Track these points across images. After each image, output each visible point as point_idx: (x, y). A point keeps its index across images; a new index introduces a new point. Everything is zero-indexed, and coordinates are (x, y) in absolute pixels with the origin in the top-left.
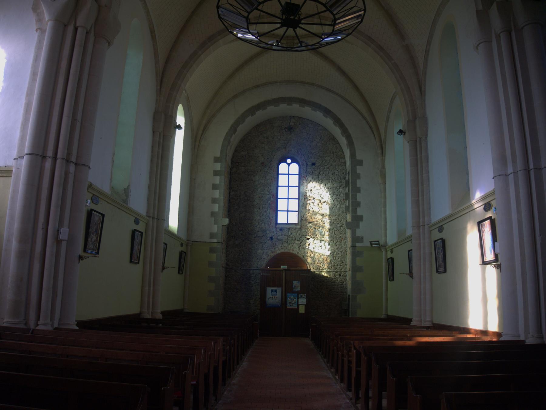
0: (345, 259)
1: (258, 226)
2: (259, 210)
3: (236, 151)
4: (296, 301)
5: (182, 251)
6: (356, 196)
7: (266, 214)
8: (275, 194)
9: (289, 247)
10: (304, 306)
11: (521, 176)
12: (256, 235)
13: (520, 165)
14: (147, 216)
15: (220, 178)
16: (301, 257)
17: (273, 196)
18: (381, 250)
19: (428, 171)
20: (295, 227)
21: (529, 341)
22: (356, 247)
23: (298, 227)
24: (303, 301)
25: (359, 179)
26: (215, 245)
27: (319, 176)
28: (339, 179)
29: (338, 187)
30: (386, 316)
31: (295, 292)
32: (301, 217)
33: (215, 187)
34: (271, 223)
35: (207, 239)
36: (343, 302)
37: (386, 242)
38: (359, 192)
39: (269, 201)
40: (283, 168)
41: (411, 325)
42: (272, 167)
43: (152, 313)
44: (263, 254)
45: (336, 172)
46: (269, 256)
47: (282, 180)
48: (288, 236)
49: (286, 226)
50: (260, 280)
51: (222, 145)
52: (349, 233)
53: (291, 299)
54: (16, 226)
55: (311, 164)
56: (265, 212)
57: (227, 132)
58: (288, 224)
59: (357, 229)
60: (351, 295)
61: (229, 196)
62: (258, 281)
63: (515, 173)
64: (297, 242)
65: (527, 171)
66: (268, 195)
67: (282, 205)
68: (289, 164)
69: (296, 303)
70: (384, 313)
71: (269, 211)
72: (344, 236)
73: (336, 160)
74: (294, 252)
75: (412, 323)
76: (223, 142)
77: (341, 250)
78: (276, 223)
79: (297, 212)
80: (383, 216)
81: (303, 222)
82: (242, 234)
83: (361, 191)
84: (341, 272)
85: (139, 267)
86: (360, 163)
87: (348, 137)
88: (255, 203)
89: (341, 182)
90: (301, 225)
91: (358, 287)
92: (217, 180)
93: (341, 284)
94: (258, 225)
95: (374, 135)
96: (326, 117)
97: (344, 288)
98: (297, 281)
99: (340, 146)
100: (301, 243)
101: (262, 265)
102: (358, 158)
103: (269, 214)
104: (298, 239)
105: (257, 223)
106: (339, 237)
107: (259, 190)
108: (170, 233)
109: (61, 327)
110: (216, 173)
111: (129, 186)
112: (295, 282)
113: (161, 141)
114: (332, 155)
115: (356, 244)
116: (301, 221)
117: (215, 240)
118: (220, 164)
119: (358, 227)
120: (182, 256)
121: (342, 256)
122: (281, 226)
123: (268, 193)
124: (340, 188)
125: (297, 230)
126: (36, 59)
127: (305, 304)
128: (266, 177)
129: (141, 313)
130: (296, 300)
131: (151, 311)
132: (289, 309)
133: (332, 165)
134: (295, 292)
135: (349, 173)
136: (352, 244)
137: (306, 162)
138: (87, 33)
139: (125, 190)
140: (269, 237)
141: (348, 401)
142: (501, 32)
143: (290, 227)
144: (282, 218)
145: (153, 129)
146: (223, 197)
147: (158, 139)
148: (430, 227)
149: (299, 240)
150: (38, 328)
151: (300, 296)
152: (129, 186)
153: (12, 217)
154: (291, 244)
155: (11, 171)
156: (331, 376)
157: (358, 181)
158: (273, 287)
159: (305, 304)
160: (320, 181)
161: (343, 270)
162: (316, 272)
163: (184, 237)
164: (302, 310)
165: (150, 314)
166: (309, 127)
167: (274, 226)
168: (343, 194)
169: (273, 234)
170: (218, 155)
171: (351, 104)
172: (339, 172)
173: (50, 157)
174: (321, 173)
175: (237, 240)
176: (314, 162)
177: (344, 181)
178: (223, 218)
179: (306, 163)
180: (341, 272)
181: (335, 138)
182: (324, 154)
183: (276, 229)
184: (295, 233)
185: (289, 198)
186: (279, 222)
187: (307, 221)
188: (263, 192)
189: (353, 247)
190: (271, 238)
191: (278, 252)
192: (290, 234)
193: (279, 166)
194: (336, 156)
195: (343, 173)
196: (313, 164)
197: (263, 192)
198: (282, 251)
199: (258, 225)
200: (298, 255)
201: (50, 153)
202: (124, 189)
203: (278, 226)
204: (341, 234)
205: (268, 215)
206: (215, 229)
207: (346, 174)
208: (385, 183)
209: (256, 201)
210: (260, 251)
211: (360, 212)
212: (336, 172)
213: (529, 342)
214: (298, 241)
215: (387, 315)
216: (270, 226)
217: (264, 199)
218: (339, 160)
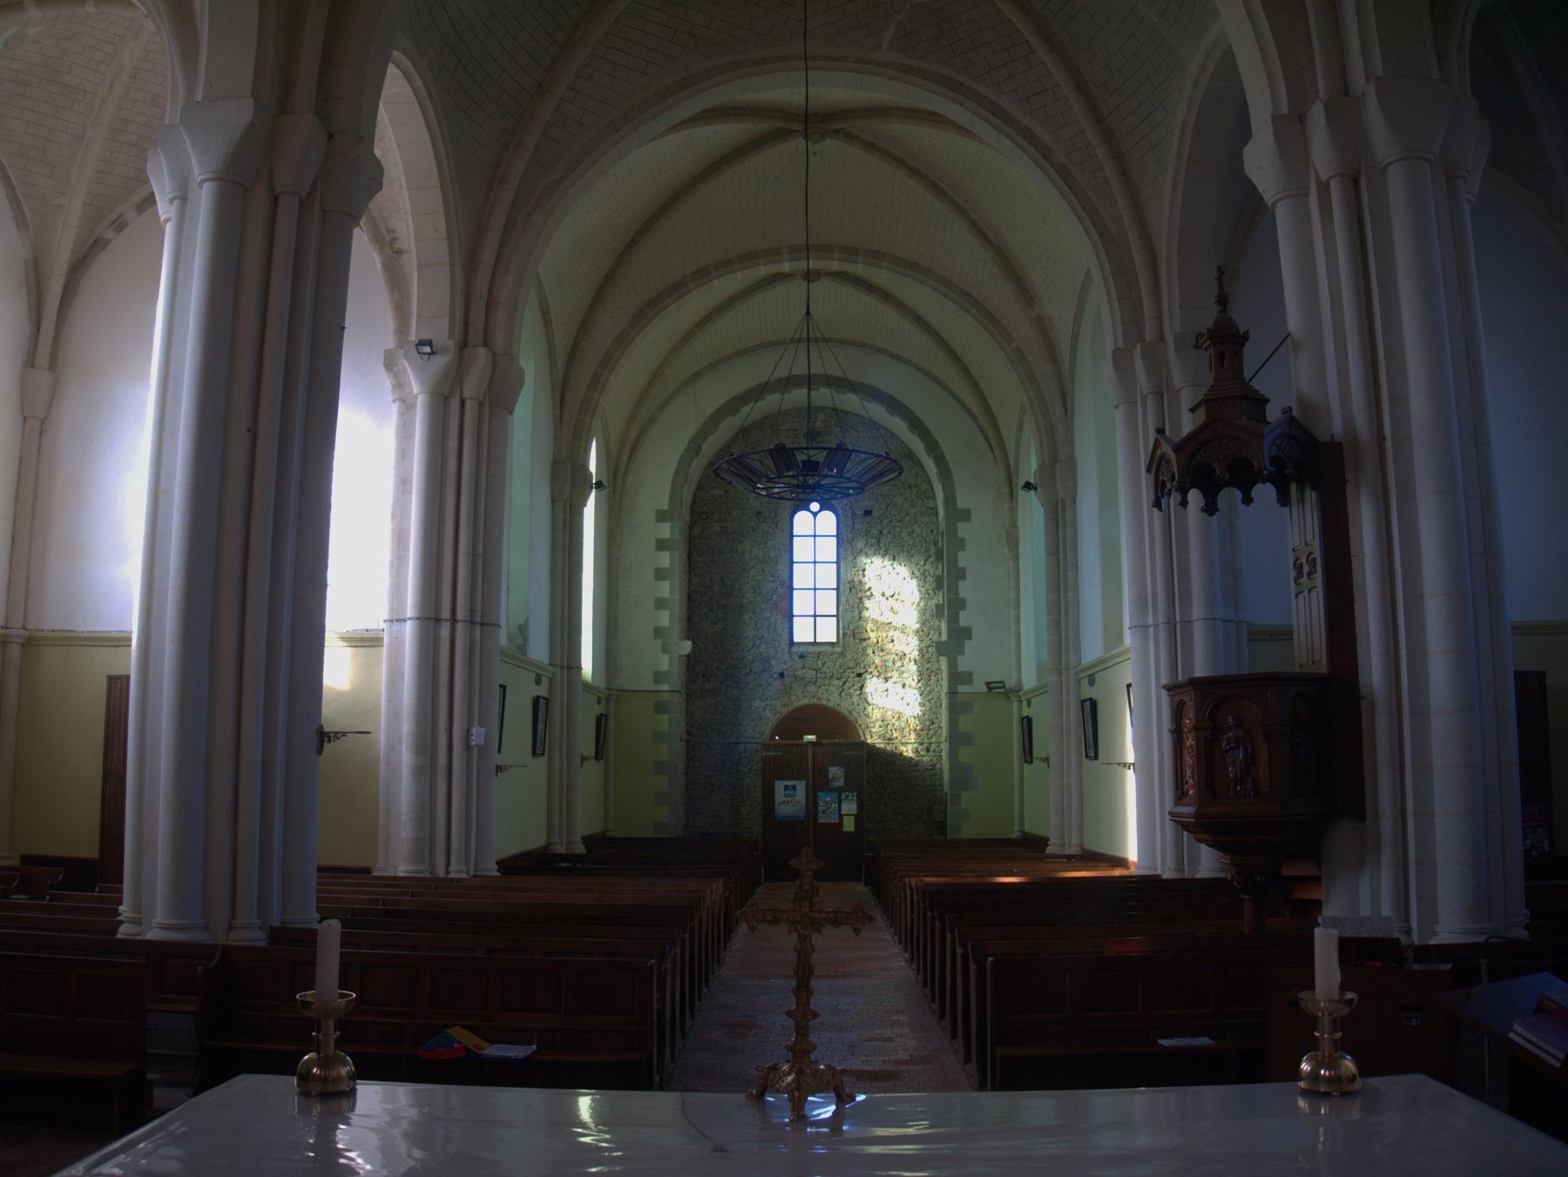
0: (939, 716)
1: (753, 651)
2: (753, 616)
3: (699, 488)
4: (837, 809)
5: (601, 715)
6: (957, 586)
7: (770, 624)
8: (787, 582)
9: (820, 692)
10: (853, 818)
11: (1163, 635)
12: (748, 670)
13: (1161, 618)
14: (550, 665)
15: (671, 556)
16: (845, 712)
17: (782, 585)
18: (1009, 699)
19: (1077, 566)
20: (830, 649)
21: (1167, 875)
22: (957, 693)
23: (838, 649)
24: (849, 807)
25: (964, 549)
26: (665, 697)
27: (879, 538)
28: (924, 545)
29: (922, 563)
30: (1021, 834)
31: (833, 790)
32: (844, 628)
33: (660, 574)
34: (779, 643)
35: (648, 684)
36: (935, 807)
37: (1020, 683)
38: (964, 578)
39: (775, 597)
40: (802, 521)
41: (1047, 852)
42: (780, 521)
43: (567, 844)
44: (765, 709)
45: (918, 530)
46: (777, 712)
47: (801, 549)
48: (816, 670)
49: (811, 649)
50: (760, 764)
51: (673, 483)
52: (944, 662)
53: (827, 803)
54: (406, 728)
55: (862, 512)
56: (768, 619)
57: (682, 456)
58: (815, 643)
59: (959, 657)
60: (948, 792)
61: (689, 586)
62: (755, 767)
63: (1156, 626)
64: (836, 682)
65: (1171, 624)
66: (773, 582)
67: (801, 603)
68: (815, 514)
69: (837, 812)
70: (1016, 828)
71: (774, 617)
72: (936, 666)
73: (917, 503)
74: (831, 704)
75: (1048, 848)
76: (674, 476)
77: (930, 697)
78: (792, 643)
79: (835, 619)
80: (1013, 628)
81: (846, 639)
82: (717, 668)
83: (968, 578)
84: (930, 744)
85: (543, 760)
86: (966, 515)
87: (940, 460)
88: (745, 601)
89: (927, 551)
90: (844, 646)
91: (963, 775)
92: (665, 559)
93: (931, 770)
94: (752, 648)
95: (994, 456)
96: (894, 416)
97: (938, 777)
98: (837, 766)
99: (926, 472)
100: (844, 683)
101: (764, 732)
102: (961, 504)
103: (776, 623)
104: (839, 676)
105: (751, 645)
106: (925, 669)
107: (752, 572)
108: (586, 685)
109: (478, 874)
110: (661, 545)
111: (526, 621)
112: (835, 768)
113: (568, 516)
114: (908, 491)
115: (956, 688)
116: (844, 637)
117: (666, 687)
118: (669, 524)
119: (961, 651)
120: (601, 721)
121: (931, 709)
122: (801, 649)
123: (771, 579)
124: (925, 565)
125: (835, 656)
126: (403, 455)
127: (855, 813)
128: (766, 543)
129: (548, 844)
130: (837, 805)
131: (565, 840)
132: (822, 824)
133: (907, 514)
134: (833, 790)
135: (942, 533)
136: (950, 688)
137: (851, 508)
138: (480, 404)
139: (520, 627)
140: (777, 673)
141: (904, 964)
142: (1149, 394)
143: (820, 650)
144: (802, 632)
145: (552, 495)
146: (678, 597)
147: (562, 515)
148: (1077, 673)
149: (840, 679)
150: (452, 875)
151: (843, 796)
152: (526, 621)
153: (394, 714)
154: (823, 687)
155: (381, 639)
156: (889, 938)
157: (960, 554)
158: (788, 779)
159: (855, 813)
160: (883, 549)
161: (934, 740)
162: (877, 745)
163: (601, 684)
164: (849, 825)
165: (564, 845)
166: (857, 431)
167: (786, 648)
168: (933, 577)
169: (785, 667)
170: (665, 506)
171: (945, 387)
172: (922, 531)
173: (447, 620)
174: (885, 531)
175: (708, 680)
176: (869, 508)
177: (932, 549)
178: (680, 639)
179: (851, 511)
180: (930, 744)
181: (914, 454)
182: (890, 490)
183: (791, 655)
184: (831, 664)
185: (817, 614)
186: (796, 639)
187: (856, 636)
188: (760, 578)
189: (952, 693)
190: (782, 675)
191: (797, 704)
192: (820, 666)
193: (796, 512)
194: (918, 493)
195: (932, 531)
196: (868, 513)
197: (760, 578)
198: (805, 701)
199: (752, 648)
200: (839, 709)
201: (446, 614)
202: (519, 626)
203: (795, 649)
204: (929, 662)
205: (773, 625)
206: (664, 663)
207: (938, 533)
208: (1016, 558)
209: (747, 596)
210: (757, 703)
211: (964, 619)
212: (918, 530)
213: (1165, 876)
214: (838, 679)
215: (1023, 832)
216: (779, 649)
217: (764, 592)
218: (923, 501)
